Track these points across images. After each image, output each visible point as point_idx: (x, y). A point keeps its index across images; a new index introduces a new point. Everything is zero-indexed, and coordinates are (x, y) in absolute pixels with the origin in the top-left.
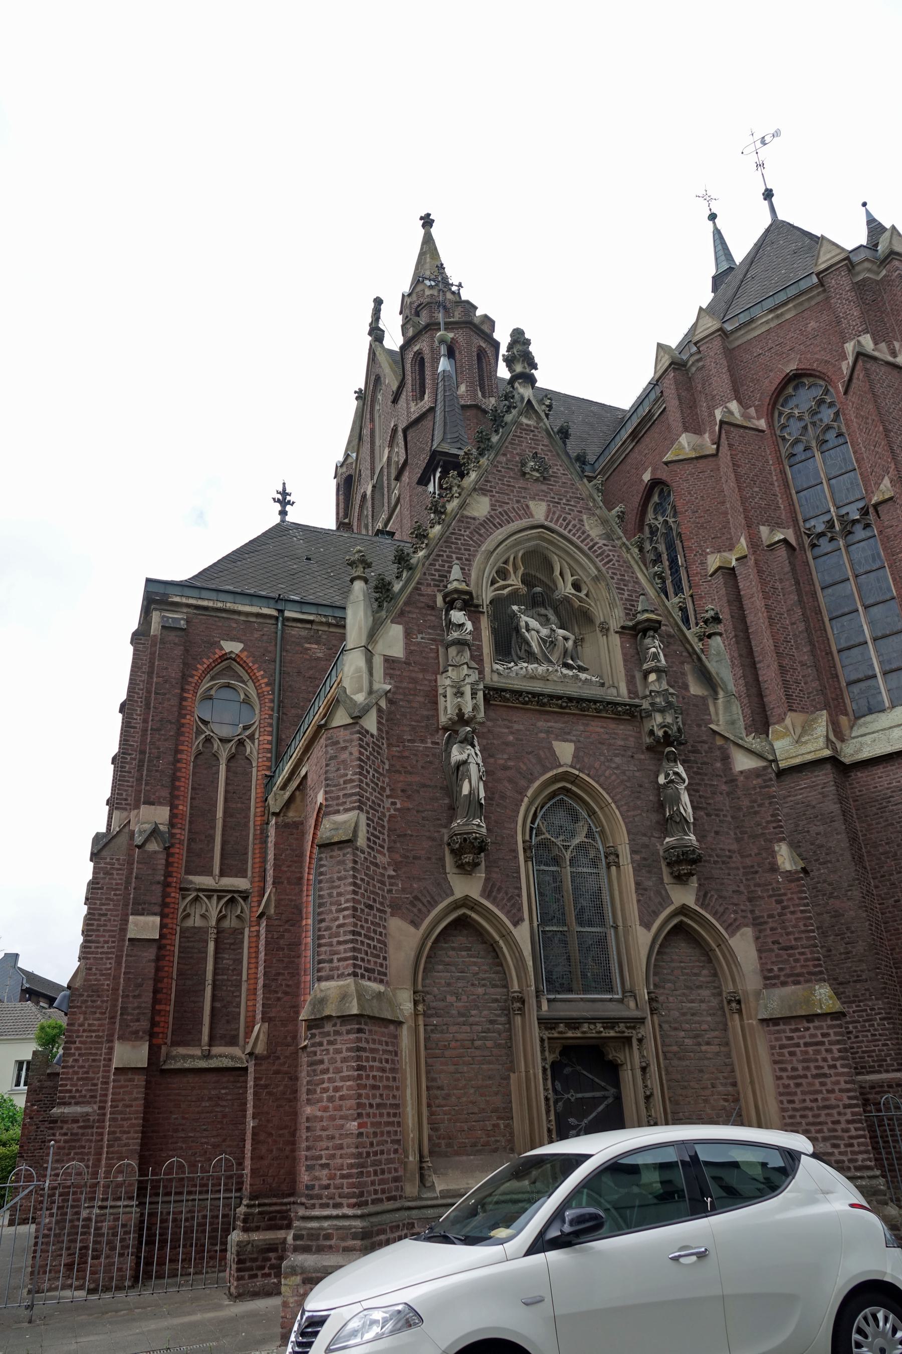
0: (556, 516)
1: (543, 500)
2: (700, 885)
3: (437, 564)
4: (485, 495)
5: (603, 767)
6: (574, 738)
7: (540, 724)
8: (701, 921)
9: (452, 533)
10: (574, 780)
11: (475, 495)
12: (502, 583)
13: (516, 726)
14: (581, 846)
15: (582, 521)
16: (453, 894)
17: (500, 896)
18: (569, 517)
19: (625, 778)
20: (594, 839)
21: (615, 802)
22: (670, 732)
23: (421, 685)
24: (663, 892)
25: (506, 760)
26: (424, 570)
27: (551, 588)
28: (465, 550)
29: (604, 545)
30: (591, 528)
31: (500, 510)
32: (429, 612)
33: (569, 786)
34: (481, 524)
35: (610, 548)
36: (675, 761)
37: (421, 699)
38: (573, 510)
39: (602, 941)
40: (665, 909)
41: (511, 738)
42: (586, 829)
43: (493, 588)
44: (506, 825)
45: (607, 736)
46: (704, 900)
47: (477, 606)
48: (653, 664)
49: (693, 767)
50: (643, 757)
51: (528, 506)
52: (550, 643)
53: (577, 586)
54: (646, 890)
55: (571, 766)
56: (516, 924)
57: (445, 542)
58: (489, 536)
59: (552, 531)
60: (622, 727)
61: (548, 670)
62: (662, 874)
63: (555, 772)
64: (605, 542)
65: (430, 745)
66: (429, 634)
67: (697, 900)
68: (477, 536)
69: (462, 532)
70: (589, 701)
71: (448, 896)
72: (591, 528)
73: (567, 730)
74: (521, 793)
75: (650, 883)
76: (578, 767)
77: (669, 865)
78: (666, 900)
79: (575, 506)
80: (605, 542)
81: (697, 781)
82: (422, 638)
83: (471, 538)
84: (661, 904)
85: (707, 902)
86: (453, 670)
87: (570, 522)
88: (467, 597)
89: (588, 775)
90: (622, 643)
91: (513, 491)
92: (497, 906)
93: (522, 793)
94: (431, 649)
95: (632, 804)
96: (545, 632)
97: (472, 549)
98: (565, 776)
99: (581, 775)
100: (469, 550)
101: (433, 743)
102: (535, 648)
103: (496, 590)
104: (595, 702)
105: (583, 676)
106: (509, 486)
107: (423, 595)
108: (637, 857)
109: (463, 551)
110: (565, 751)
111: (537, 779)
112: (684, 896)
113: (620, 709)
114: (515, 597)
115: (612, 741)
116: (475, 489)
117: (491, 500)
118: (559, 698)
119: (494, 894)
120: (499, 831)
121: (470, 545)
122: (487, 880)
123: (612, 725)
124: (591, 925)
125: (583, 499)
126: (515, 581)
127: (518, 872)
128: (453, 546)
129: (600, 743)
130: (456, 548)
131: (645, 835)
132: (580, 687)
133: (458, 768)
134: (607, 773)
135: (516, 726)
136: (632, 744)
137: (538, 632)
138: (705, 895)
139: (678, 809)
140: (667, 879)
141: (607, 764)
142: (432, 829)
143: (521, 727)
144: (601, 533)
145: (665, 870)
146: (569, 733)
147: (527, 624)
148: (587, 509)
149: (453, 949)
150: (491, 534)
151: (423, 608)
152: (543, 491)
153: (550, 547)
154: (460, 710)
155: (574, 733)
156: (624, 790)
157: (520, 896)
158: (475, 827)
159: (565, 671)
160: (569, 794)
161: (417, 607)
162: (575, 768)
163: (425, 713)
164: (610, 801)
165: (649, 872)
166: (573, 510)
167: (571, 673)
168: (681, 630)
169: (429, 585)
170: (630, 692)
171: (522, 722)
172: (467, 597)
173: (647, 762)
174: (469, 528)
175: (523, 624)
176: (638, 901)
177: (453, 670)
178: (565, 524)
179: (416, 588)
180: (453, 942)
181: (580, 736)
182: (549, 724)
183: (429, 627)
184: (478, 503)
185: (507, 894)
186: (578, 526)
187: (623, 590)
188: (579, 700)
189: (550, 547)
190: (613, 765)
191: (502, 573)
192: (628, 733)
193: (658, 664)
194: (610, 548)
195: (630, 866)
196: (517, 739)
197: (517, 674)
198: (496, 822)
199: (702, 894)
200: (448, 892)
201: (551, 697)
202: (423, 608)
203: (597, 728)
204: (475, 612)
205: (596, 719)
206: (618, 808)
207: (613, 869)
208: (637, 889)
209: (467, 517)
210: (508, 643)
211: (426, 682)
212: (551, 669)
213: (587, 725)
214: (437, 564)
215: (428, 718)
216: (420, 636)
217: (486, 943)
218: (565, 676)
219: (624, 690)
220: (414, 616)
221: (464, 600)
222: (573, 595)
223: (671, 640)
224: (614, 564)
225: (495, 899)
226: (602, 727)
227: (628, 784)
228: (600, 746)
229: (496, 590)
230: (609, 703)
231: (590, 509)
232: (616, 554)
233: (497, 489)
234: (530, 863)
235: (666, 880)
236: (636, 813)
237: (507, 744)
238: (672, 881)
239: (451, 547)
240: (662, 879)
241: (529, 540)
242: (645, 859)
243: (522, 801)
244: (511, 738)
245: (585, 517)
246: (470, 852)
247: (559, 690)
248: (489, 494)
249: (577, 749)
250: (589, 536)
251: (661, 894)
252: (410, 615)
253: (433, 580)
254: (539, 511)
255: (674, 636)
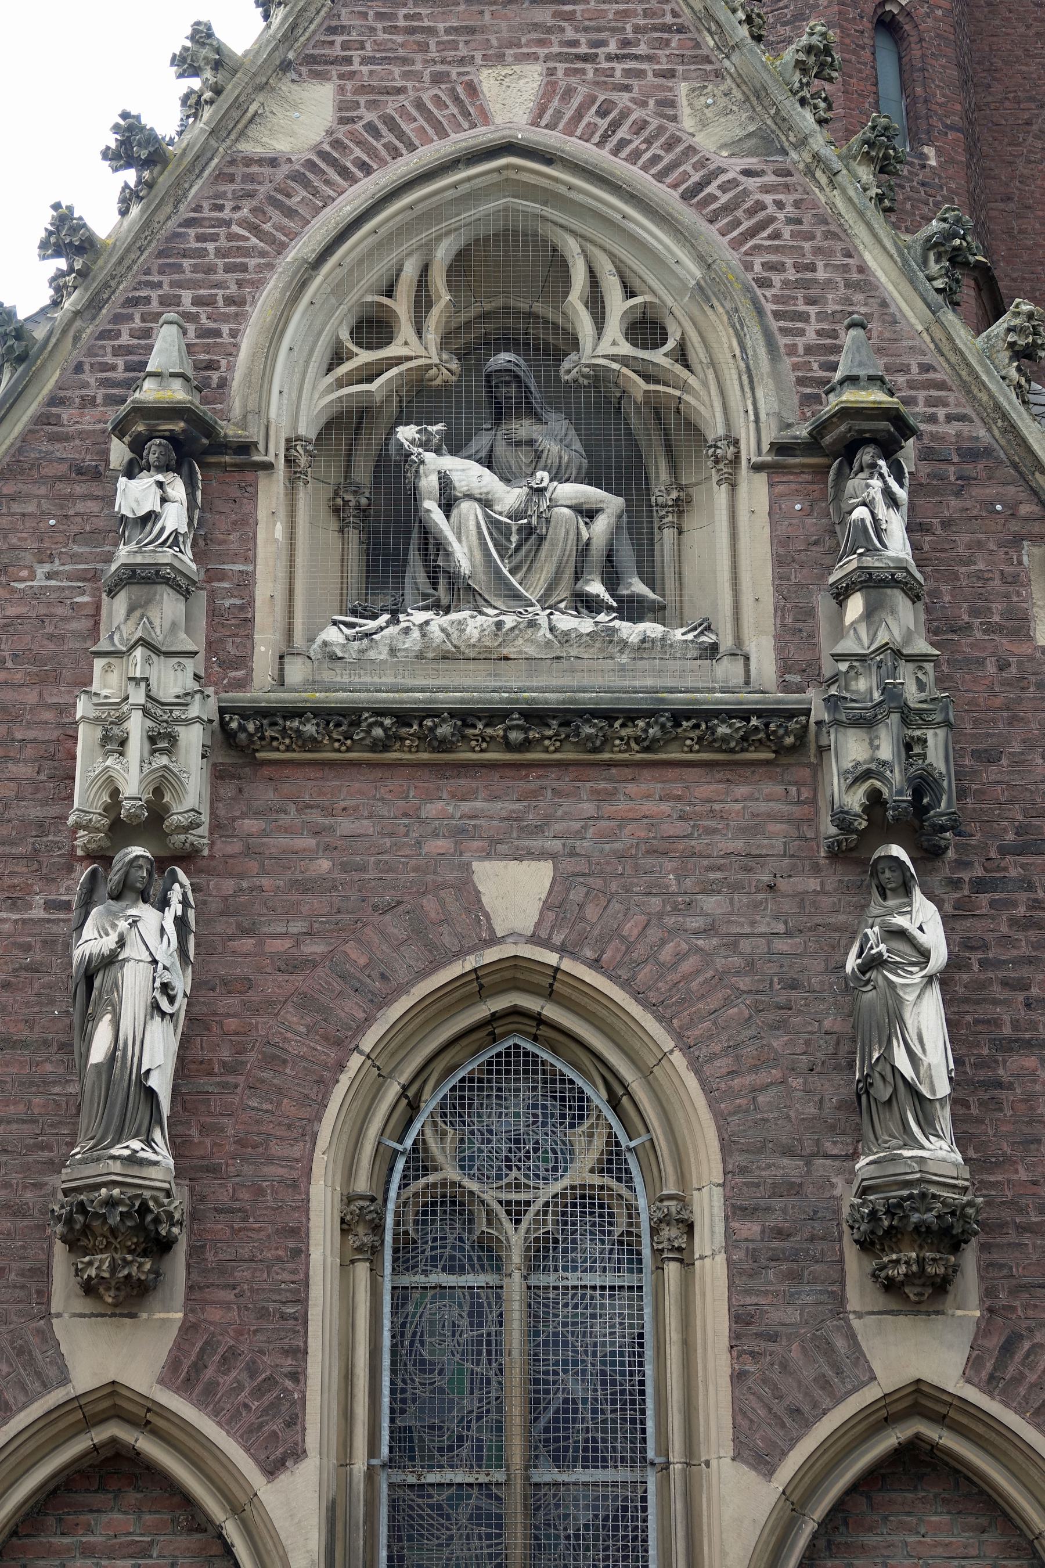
0: (576, 102)
1: (534, 58)
2: (991, 1310)
3: (125, 329)
4: (320, 76)
5: (654, 934)
6: (556, 845)
7: (432, 809)
8: (981, 1429)
9: (189, 223)
10: (550, 984)
11: (285, 86)
12: (365, 357)
13: (346, 826)
14: (584, 1202)
15: (672, 104)
16: (65, 1380)
17: (226, 1381)
18: (623, 99)
19: (736, 961)
20: (623, 1175)
21: (686, 1048)
22: (885, 791)
23: (29, 725)
24: (840, 1344)
25: (298, 939)
26: (77, 356)
27: (549, 344)
28: (229, 269)
29: (747, 173)
30: (704, 124)
31: (370, 116)
32: (79, 489)
33: (531, 1003)
34: (297, 177)
35: (770, 179)
36: (908, 893)
37: (25, 771)
38: (640, 74)
39: (625, 1520)
40: (838, 1401)
41: (324, 865)
42: (599, 1142)
43: (330, 379)
44: (276, 1149)
45: (681, 827)
46: (1001, 1363)
47: (245, 448)
48: (852, 563)
49: (1015, 904)
50: (813, 884)
51: (472, 89)
52: (522, 537)
53: (646, 329)
54: (773, 1337)
55: (534, 940)
56: (273, 1469)
57: (161, 254)
58: (318, 210)
59: (548, 158)
60: (741, 790)
61: (499, 625)
62: (842, 1282)
63: (471, 962)
64: (752, 162)
65: (38, 913)
66: (74, 558)
67: (974, 1364)
68: (277, 217)
69: (227, 214)
70: (608, 715)
71: (47, 1387)
72: (704, 124)
73: (531, 819)
74: (338, 1043)
75: (793, 1316)
76: (558, 939)
77: (865, 1245)
78: (856, 1367)
79: (649, 58)
80: (752, 162)
81: (1025, 950)
82: (49, 576)
83: (255, 229)
84: (824, 1383)
85: (1011, 1371)
86: (107, 669)
87: (624, 115)
88: (179, 426)
89: (595, 964)
90: (774, 502)
91: (424, 47)
92: (215, 1414)
93: (343, 1043)
94: (74, 606)
95: (749, 1051)
96: (509, 497)
97: (252, 262)
98: (514, 974)
99: (567, 965)
100: (243, 268)
101: (49, 906)
102: (463, 555)
103: (340, 383)
104: (630, 716)
105: (631, 631)
106: (411, 31)
107: (66, 438)
108: (751, 1229)
109: (220, 276)
110: (514, 893)
111: (401, 990)
112: (931, 1353)
113: (723, 730)
114: (417, 399)
115: (698, 843)
116: (286, 66)
117: (342, 89)
118: (494, 716)
119: (209, 1373)
120: (248, 1170)
121: (246, 252)
122: (188, 1329)
123: (705, 788)
124: (594, 1458)
125: (681, 30)
126: (416, 347)
127: (302, 1300)
128: (187, 263)
129: (652, 852)
130: (195, 269)
131: (788, 1152)
132: (622, 668)
133: (89, 979)
134: (666, 954)
135: (346, 826)
136: (778, 844)
137: (486, 503)
138: (1008, 1348)
139: (887, 1057)
140: (858, 1291)
141: (669, 921)
142: (16, 1178)
143: (365, 826)
144: (740, 133)
145: (855, 1265)
146: (538, 830)
147: (445, 481)
148: (696, 59)
149: (88, 1551)
150: (327, 201)
151: (60, 479)
152: (536, 27)
153: (548, 211)
154: (115, 793)
155: (559, 827)
156: (727, 1003)
157: (298, 1376)
158: (116, 1167)
159: (566, 622)
160: (544, 1031)
161: (43, 480)
162: (545, 944)
163: (35, 812)
164: (667, 1043)
165: (794, 1277)
166: (640, 74)
167: (586, 625)
168: (1011, 429)
169: (89, 402)
170: (785, 665)
171: (364, 811)
172: (179, 426)
173: (826, 901)
174: (251, 195)
175: (429, 483)
176: (738, 1377)
177: (107, 669)
178: (603, 124)
179: (43, 419)
180: (89, 1530)
181: (580, 834)
182: (467, 807)
183: (75, 538)
184: (295, 106)
185: (252, 1371)
186: (655, 123)
187: (804, 317)
188: (568, 717)
189: (548, 211)
190: (695, 923)
191: (373, 328)
192: (763, 807)
193: (869, 561)
194: (770, 179)
195: (721, 1258)
196: (345, 867)
197: (393, 651)
198: (241, 1142)
199: (994, 1342)
200: (52, 1372)
201: (465, 717)
202: (60, 479)
203: (645, 802)
204: (240, 467)
205: (646, 773)
206: (696, 1066)
207: (672, 1269)
208: (736, 1337)
209: (249, 161)
210: (392, 550)
211: (47, 715)
212: (509, 621)
213: (611, 794)
214: (125, 329)
215: (42, 828)
216: (41, 570)
217: (201, 1529)
218: (565, 638)
219: (765, 663)
220: (31, 508)
221: (172, 438)
222: (624, 360)
223: (977, 469)
224: (776, 235)
225: (210, 1389)
226: (664, 798)
227: (744, 983)
228: (649, 861)
229: (340, 383)
230: (678, 716)
231: (707, 60)
232: (788, 198)
233: (369, 50)
234: (362, 1270)
235: (854, 1301)
236: (763, 1077)
237: (305, 886)
238: (881, 1301)
239: (178, 268)
240: (841, 1299)
241: (473, 197)
242: (781, 1234)
243: (341, 1067)
244: (324, 865)
245: (683, 88)
246: (125, 1249)
247: (546, 688)
248: (334, 71)
249: (561, 881)
250: (691, 149)
251: (829, 1350)
252: (16, 508)
253: (104, 383)
254: (512, 98)
255: (988, 452)
